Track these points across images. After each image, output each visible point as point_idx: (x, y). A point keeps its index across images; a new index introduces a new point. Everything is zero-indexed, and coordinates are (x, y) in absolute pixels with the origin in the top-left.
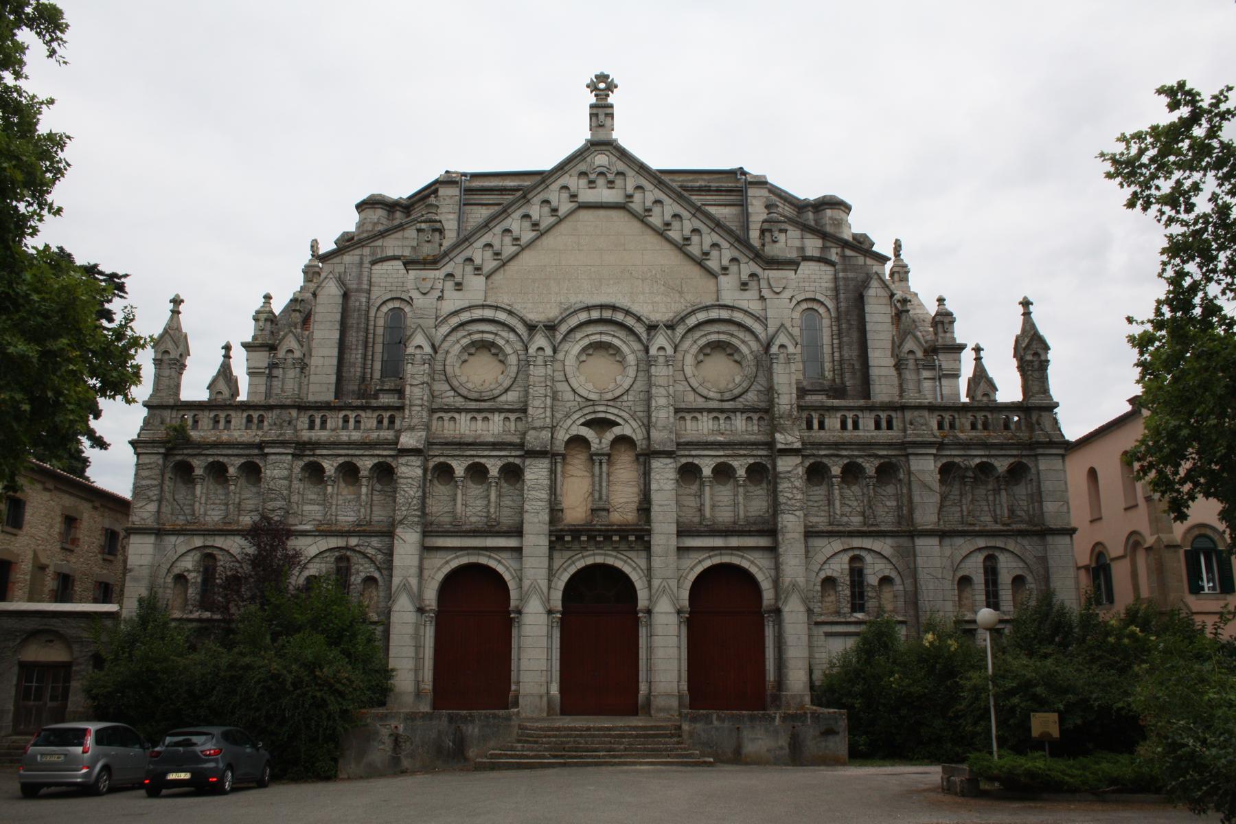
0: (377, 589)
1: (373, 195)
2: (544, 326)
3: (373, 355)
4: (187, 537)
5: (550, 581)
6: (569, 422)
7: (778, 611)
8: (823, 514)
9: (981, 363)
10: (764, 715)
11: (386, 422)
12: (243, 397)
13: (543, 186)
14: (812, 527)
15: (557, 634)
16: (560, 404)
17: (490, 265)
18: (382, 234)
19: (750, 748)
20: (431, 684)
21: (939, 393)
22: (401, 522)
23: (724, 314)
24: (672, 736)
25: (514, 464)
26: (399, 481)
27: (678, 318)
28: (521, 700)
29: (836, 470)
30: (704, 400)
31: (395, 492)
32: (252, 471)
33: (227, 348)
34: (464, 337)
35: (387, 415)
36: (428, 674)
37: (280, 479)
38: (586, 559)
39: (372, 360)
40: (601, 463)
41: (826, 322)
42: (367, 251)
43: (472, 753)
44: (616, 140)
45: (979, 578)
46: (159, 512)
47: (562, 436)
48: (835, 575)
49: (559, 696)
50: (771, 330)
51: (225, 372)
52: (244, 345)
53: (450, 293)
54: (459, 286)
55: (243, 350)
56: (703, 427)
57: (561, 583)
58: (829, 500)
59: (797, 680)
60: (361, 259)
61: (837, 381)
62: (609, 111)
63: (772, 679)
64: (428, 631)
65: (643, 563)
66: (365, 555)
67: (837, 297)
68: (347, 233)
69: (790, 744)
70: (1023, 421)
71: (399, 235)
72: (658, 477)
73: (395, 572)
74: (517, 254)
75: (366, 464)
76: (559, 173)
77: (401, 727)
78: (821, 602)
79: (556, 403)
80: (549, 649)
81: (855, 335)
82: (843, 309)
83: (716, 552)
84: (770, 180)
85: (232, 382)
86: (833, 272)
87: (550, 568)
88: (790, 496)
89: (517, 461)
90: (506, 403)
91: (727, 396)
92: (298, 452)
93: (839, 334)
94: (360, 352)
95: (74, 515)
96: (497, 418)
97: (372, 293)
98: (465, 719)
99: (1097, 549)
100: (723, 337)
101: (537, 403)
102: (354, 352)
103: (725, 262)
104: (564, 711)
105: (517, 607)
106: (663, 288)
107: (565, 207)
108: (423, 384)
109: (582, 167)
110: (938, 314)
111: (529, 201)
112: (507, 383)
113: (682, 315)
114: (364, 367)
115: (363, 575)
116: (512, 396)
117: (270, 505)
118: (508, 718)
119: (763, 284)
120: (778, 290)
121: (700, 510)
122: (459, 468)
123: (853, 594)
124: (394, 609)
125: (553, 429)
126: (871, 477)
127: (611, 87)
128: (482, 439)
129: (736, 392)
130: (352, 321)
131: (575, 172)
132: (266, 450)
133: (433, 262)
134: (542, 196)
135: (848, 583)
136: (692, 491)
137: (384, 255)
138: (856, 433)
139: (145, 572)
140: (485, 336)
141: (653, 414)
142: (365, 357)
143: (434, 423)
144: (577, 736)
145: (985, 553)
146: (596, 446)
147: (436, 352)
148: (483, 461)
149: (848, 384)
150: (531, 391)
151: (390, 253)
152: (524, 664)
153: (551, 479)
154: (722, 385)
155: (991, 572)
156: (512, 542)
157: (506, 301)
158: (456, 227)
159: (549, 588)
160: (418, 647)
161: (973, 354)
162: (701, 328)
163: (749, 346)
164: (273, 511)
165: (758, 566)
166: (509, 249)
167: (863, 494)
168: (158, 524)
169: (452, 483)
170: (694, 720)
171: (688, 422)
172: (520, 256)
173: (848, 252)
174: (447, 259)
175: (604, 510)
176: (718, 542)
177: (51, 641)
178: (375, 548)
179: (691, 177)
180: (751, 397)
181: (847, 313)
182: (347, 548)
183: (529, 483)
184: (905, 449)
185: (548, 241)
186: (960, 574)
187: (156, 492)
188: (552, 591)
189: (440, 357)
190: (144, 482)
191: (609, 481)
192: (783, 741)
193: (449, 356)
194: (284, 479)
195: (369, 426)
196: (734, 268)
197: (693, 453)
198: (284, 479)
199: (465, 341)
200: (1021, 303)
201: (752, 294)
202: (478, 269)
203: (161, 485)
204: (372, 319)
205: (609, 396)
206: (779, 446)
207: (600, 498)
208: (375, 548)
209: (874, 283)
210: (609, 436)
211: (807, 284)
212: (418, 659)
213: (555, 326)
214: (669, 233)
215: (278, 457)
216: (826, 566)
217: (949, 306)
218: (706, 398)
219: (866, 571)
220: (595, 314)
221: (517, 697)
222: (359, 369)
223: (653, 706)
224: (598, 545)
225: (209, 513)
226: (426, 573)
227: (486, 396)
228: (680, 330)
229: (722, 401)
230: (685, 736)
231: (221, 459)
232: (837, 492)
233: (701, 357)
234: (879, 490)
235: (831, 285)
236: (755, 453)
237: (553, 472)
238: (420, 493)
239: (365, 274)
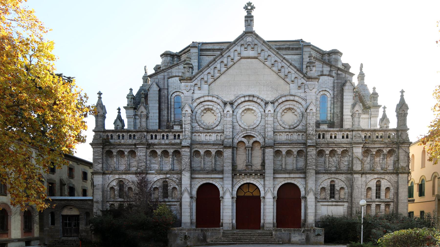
0: (177, 191)
1: (166, 51)
2: (229, 103)
3: (171, 112)
4: (113, 175)
5: (232, 188)
6: (238, 136)
7: (305, 198)
8: (322, 167)
9: (385, 113)
10: (298, 229)
11: (177, 137)
12: (126, 127)
13: (228, 50)
14: (319, 171)
15: (235, 204)
16: (235, 130)
17: (211, 80)
18: (171, 67)
20: (195, 220)
21: (369, 123)
22: (184, 170)
23: (292, 98)
24: (270, 235)
25: (220, 151)
26: (182, 156)
27: (276, 100)
28: (223, 225)
29: (327, 152)
30: (284, 129)
31: (181, 160)
32: (133, 153)
33: (119, 109)
34: (202, 107)
35: (177, 134)
36: (194, 217)
37: (143, 156)
38: (292, 181)
39: (171, 114)
40: (249, 150)
41: (329, 99)
42: (166, 74)
43: (208, 240)
44: (254, 31)
45: (374, 188)
46: (103, 167)
47: (236, 141)
48: (325, 186)
49: (235, 223)
50: (308, 104)
51: (119, 118)
52: (125, 108)
53: (197, 91)
54: (200, 88)
55: (124, 109)
56: (283, 137)
57: (236, 188)
58: (325, 162)
59: (311, 219)
60: (164, 77)
61: (332, 120)
62: (252, 19)
63: (303, 219)
64: (194, 204)
65: (262, 183)
66: (173, 180)
67: (334, 90)
68: (158, 65)
69: (306, 238)
70: (395, 135)
71: (177, 67)
72: (267, 155)
73: (183, 186)
74: (219, 77)
75: (171, 151)
76: (234, 45)
77: (187, 233)
78: (320, 195)
79: (234, 130)
80: (232, 209)
81: (339, 104)
82: (335, 94)
83: (286, 179)
84: (312, 44)
85: (122, 121)
86: (333, 80)
87: (232, 184)
88: (311, 161)
89: (221, 150)
90: (217, 130)
91: (292, 127)
92: (148, 147)
93: (334, 103)
94: (166, 111)
95: (72, 167)
96: (214, 135)
97: (169, 90)
98: (206, 230)
99: (422, 178)
100: (291, 106)
102: (164, 111)
103: (293, 79)
104: (237, 228)
105: (222, 196)
106: (270, 89)
107: (237, 58)
108: (188, 124)
109: (242, 42)
110: (373, 94)
111: (223, 56)
112: (217, 123)
113: (277, 99)
114: (168, 116)
115: (172, 187)
116: (219, 128)
117: (140, 165)
118: (219, 230)
119: (306, 87)
120: (311, 89)
121: (281, 165)
122: (202, 152)
123: (331, 193)
124: (183, 197)
125: (233, 138)
126: (339, 155)
127: (253, 8)
128: (209, 143)
129: (295, 126)
130: (163, 100)
131: (239, 44)
132: (137, 146)
133: (191, 79)
134: (228, 54)
135: (329, 189)
136: (279, 159)
137: (172, 75)
138: (335, 139)
139: (100, 187)
140: (209, 106)
141: (266, 134)
142: (168, 113)
143: (193, 137)
144: (241, 235)
145: (377, 180)
146: (247, 144)
147: (193, 112)
148: (210, 150)
149: (335, 121)
150: (225, 126)
151: (174, 75)
152: (224, 214)
153: (232, 156)
154: (290, 123)
155: (378, 187)
156: (220, 176)
157: (216, 94)
158: (197, 65)
159: (232, 190)
160: (191, 209)
161: (383, 110)
162: (284, 103)
163: (299, 109)
164: (141, 166)
165: (300, 184)
166: (217, 75)
167: (337, 160)
168: (103, 171)
169: (200, 157)
170: (276, 231)
171: (278, 136)
172: (220, 77)
173: (339, 72)
174: (195, 79)
175: (250, 165)
176: (287, 176)
177: (72, 208)
178: (176, 178)
179: (283, 43)
180: (300, 127)
181: (337, 95)
182: (166, 178)
183: (225, 157)
184: (352, 145)
185: (230, 71)
186: (368, 187)
187: (101, 161)
188: (233, 191)
189: (194, 114)
190: (97, 157)
191: (251, 156)
192: (304, 237)
193: (197, 114)
194: (144, 156)
195: (171, 138)
196: (296, 81)
197: (280, 147)
198: (144, 156)
199: (202, 108)
200: (400, 92)
201: (302, 90)
202: (206, 82)
203: (102, 159)
204: (169, 99)
205: (252, 127)
206: (308, 144)
207: (249, 162)
208: (176, 178)
209: (348, 84)
210: (252, 141)
211: (323, 85)
212: (191, 212)
213: (233, 103)
214: (273, 68)
215: (141, 149)
216: (322, 184)
217: (377, 91)
218: (284, 128)
219: (335, 186)
220: (247, 99)
221: (222, 224)
222: (166, 117)
223: (265, 227)
224: (249, 177)
225: (119, 167)
226: (193, 186)
227: (211, 127)
228: (276, 104)
229: (290, 129)
230: (273, 236)
231: (122, 149)
232: (327, 160)
233: (283, 113)
234: (342, 159)
235: (332, 85)
236: (300, 146)
237: (233, 153)
238: (189, 161)
239: (166, 82)
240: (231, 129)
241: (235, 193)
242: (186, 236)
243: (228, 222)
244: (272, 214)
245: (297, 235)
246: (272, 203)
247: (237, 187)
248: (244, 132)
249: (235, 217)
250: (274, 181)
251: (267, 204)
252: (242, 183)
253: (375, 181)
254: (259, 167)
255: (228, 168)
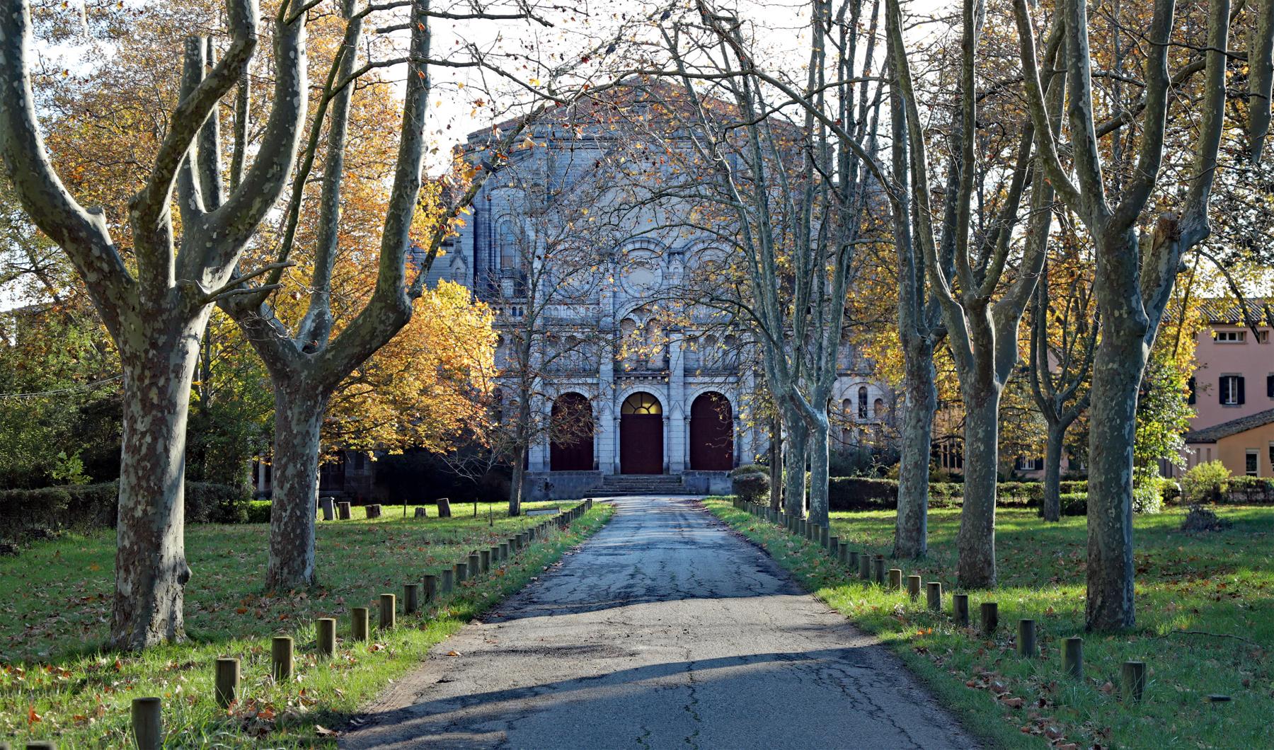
15: (618, 430)
19: (713, 488)
45: (855, 400)
47: (620, 316)
65: (665, 392)
80: (615, 438)
101: (605, 301)
104: (622, 473)
130: (481, 231)
142: (490, 256)
145: (860, 386)
152: (601, 447)
155: (863, 397)
170: (687, 474)
186: (844, 398)
240: (611, 300)
241: (618, 409)
242: (547, 484)
243: (607, 461)
244: (682, 447)
245: (718, 481)
246: (682, 428)
247: (623, 399)
248: (633, 304)
249: (688, 453)
250: (685, 388)
251: (674, 429)
252: (631, 392)
253: (857, 389)
254: (660, 364)
255: (607, 368)
